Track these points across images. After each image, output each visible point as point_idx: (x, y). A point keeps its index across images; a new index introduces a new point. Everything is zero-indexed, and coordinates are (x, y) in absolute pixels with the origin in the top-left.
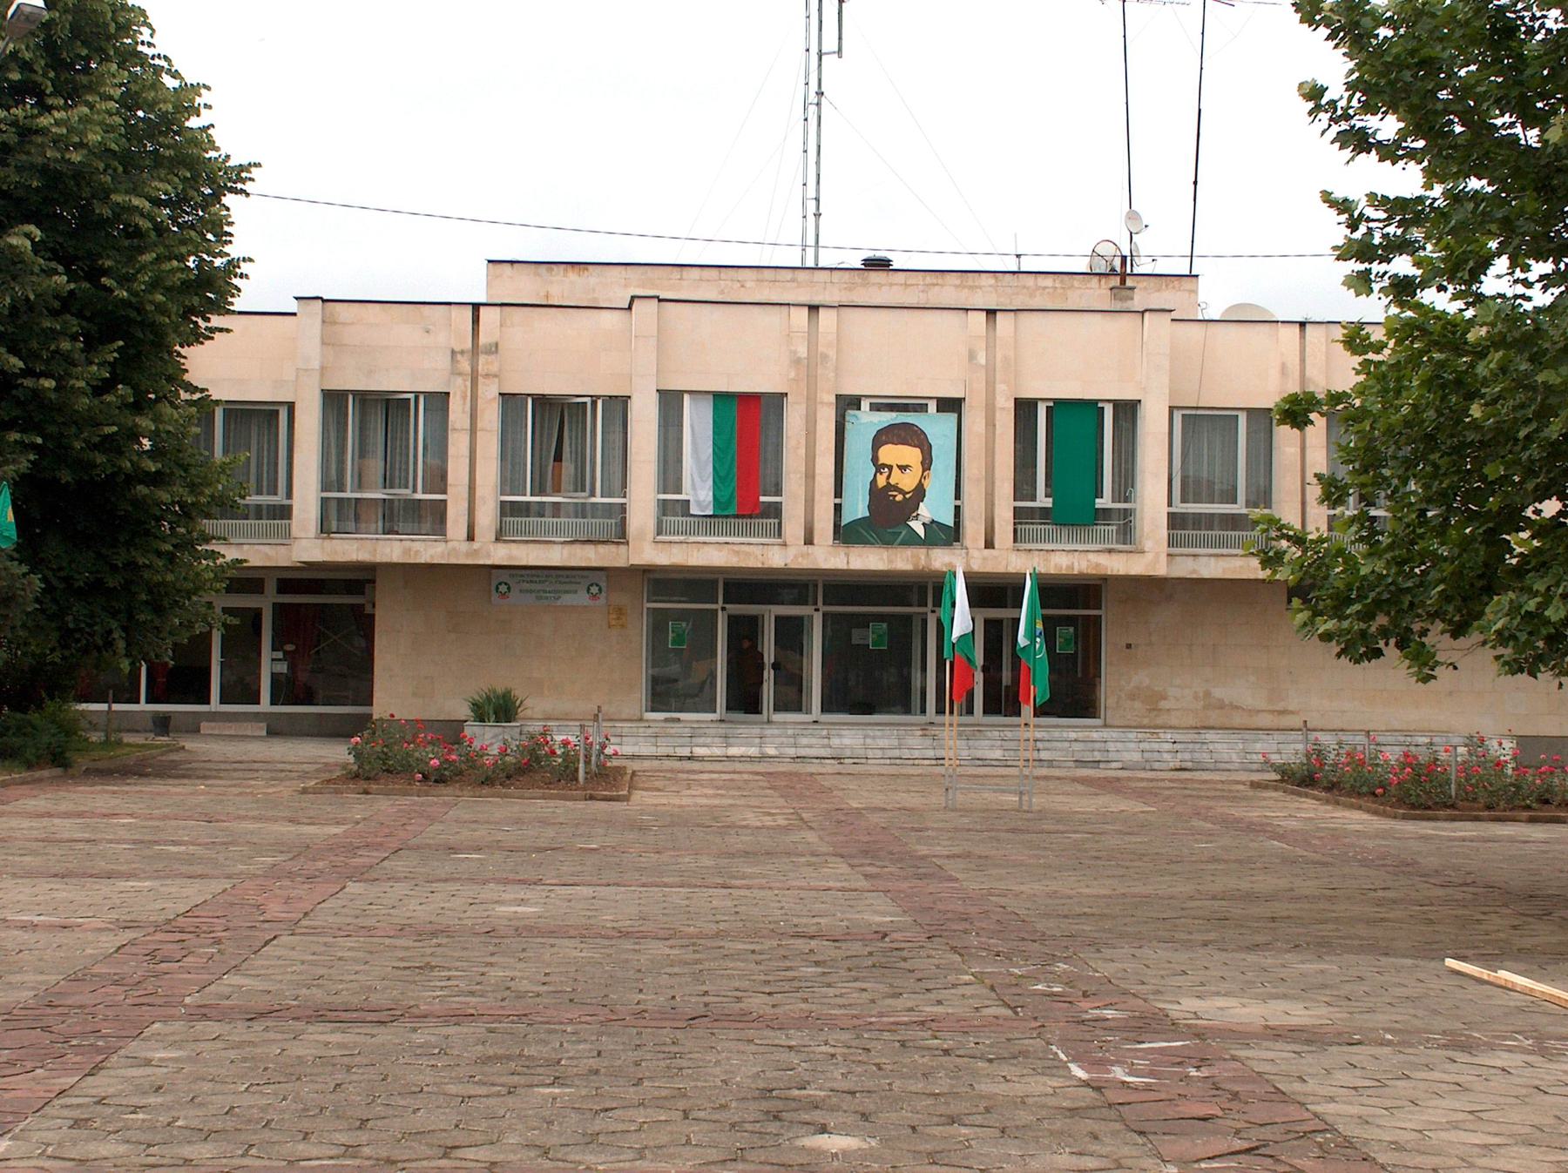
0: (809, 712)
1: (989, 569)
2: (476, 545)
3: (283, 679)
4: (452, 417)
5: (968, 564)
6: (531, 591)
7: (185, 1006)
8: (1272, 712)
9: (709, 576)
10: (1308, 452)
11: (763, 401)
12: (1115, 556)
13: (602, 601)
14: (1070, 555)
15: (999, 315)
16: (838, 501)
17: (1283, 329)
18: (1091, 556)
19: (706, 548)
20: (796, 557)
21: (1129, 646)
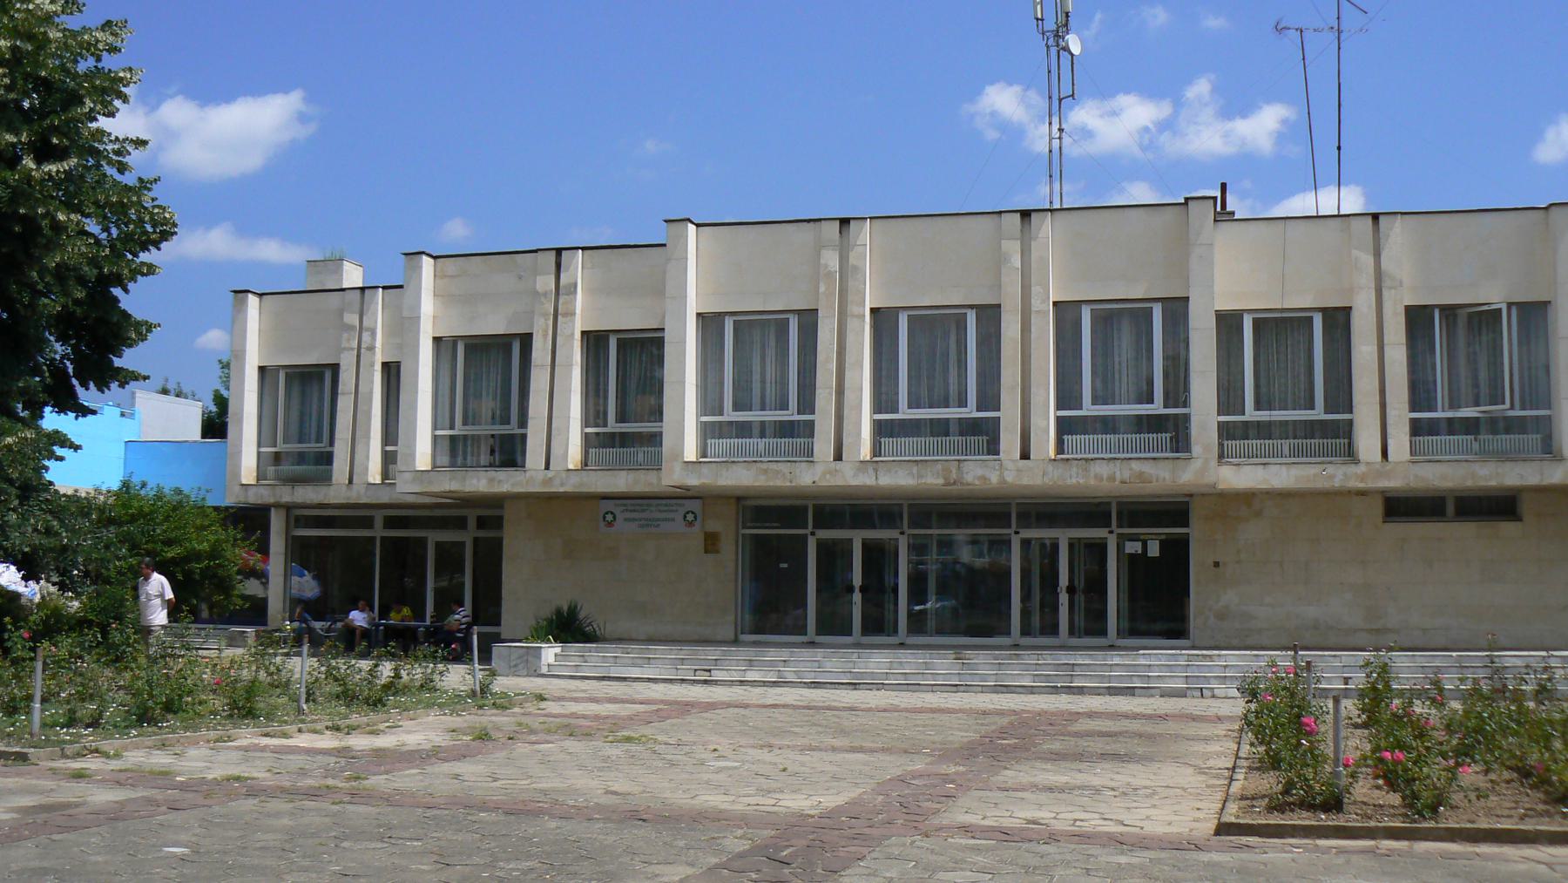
0: (1008, 633)
1: (1026, 481)
2: (550, 474)
3: (361, 604)
4: (534, 354)
5: (1001, 476)
6: (634, 520)
7: (1520, 706)
8: (1370, 631)
9: (798, 502)
10: (1386, 349)
11: (1132, 396)
12: (1162, 464)
13: (697, 528)
14: (1111, 464)
15: (1034, 215)
16: (1450, 509)
17: (1354, 222)
18: (1135, 465)
19: (734, 467)
20: (824, 474)
21: (1217, 564)
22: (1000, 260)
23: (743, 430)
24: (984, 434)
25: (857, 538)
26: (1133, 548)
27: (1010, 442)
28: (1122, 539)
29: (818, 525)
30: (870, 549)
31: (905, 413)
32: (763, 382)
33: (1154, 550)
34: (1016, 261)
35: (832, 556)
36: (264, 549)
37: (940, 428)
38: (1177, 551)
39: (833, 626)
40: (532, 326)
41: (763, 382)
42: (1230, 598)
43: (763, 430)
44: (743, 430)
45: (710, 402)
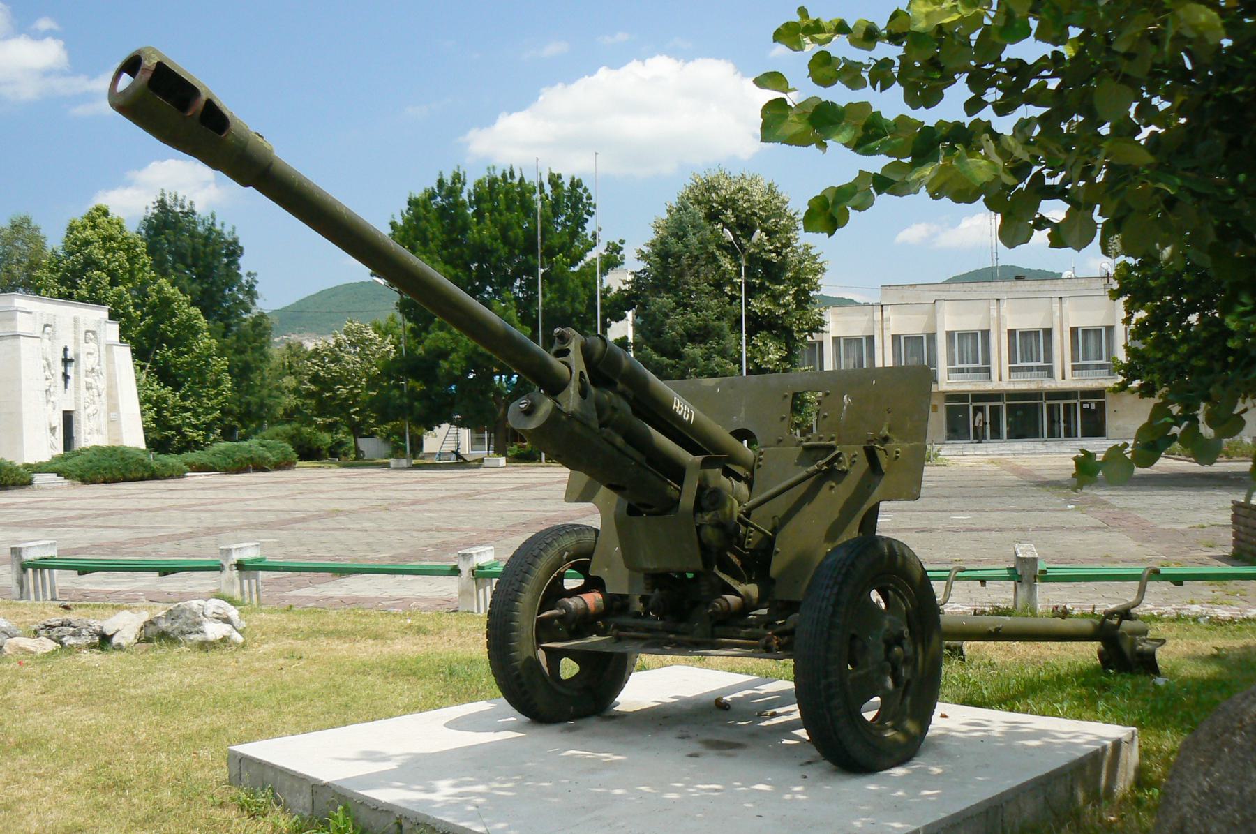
22: (1052, 314)
23: (961, 371)
24: (1050, 372)
25: (1062, 403)
26: (1086, 406)
27: (995, 376)
28: (1082, 404)
29: (1047, 399)
30: (1067, 407)
31: (1019, 364)
32: (69, 499)
33: (1093, 407)
34: (1058, 314)
35: (1050, 408)
36: (404, 441)
37: (1030, 369)
38: (1101, 406)
39: (1052, 434)
40: (935, 327)
41: (69, 499)
42: (1120, 422)
43: (968, 370)
44: (961, 371)
45: (951, 360)
